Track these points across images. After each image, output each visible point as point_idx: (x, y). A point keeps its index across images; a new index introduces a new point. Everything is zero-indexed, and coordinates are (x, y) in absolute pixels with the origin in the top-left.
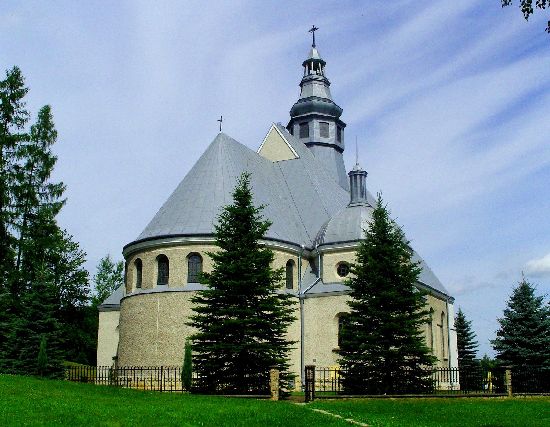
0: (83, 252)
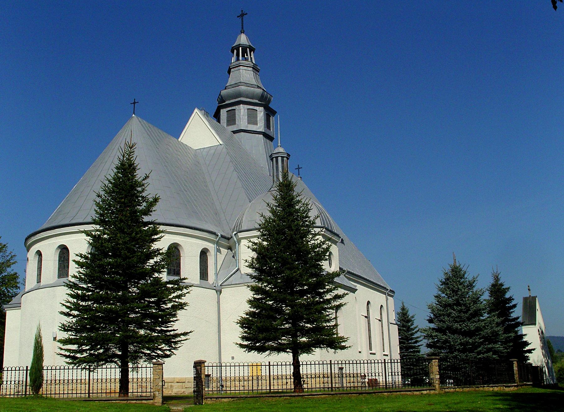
0: (13, 254)
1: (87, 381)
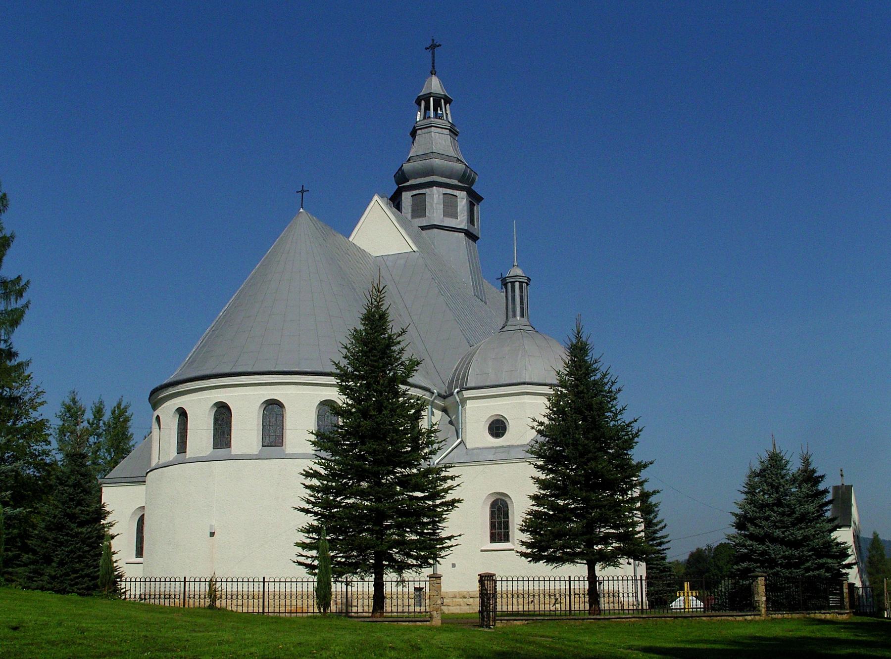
0: (39, 390)
1: (261, 593)
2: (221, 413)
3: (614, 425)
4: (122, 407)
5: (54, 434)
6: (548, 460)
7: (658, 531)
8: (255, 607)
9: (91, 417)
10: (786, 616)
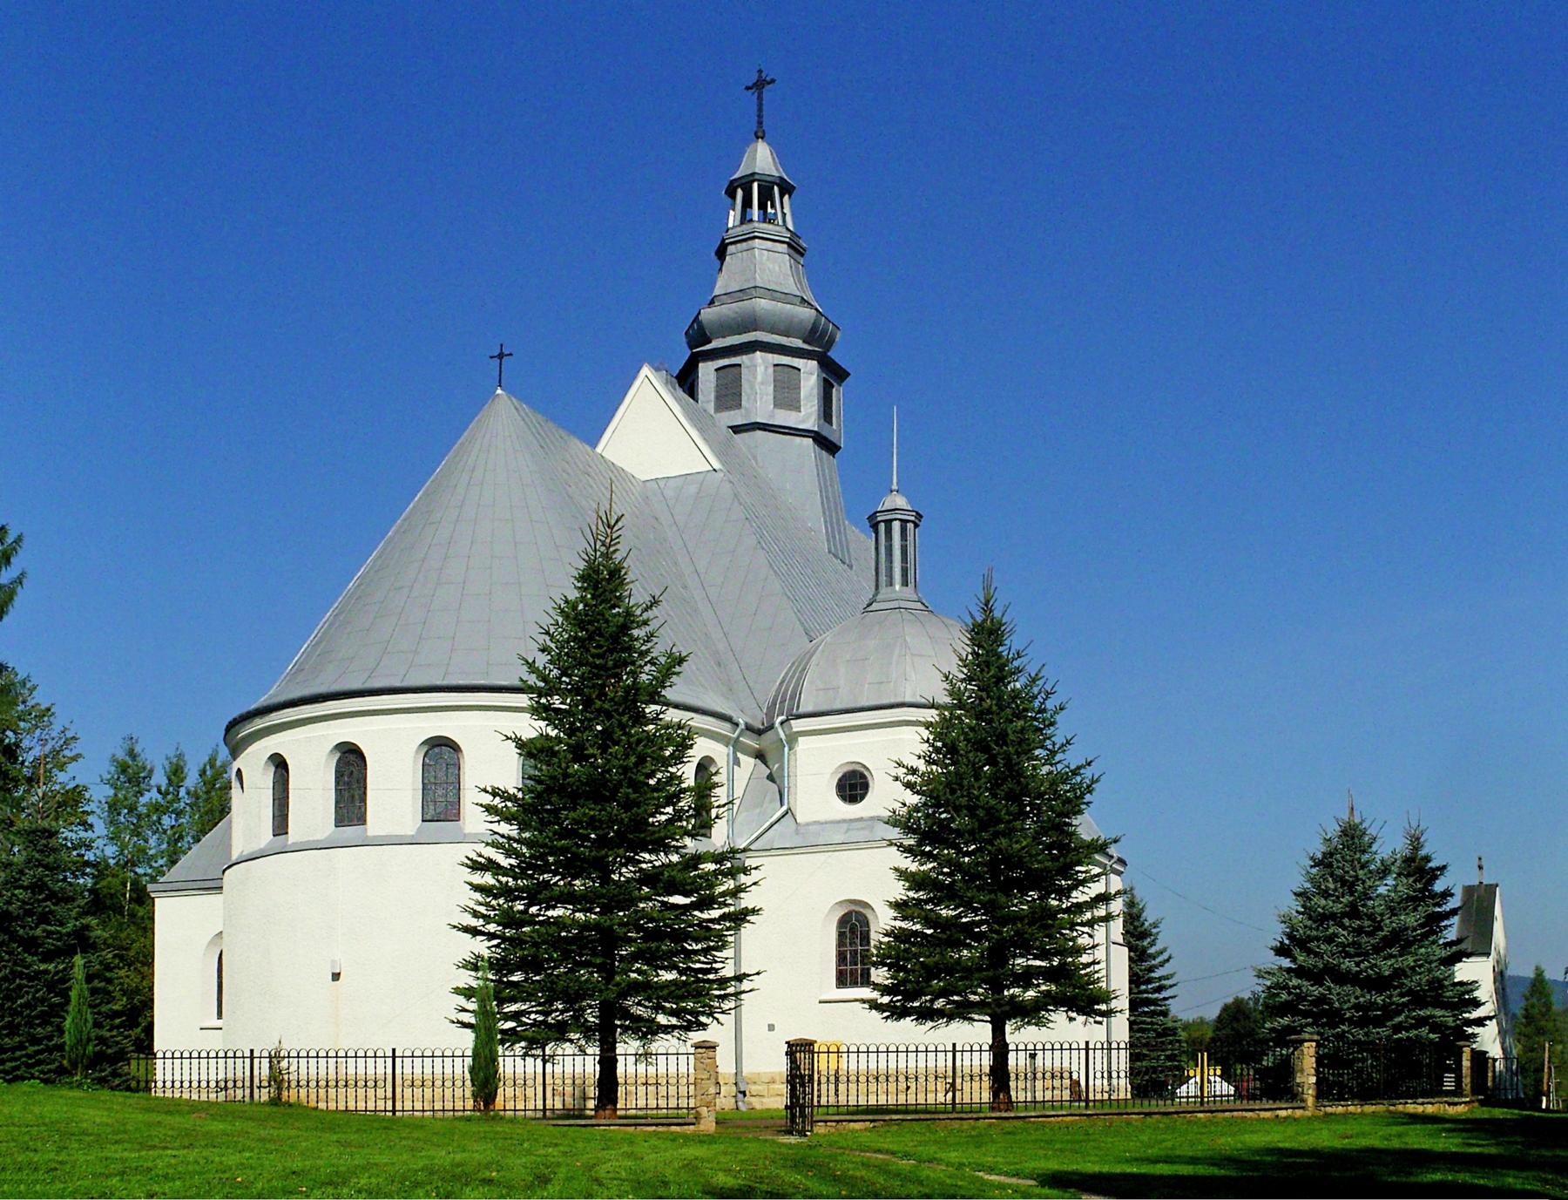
0: (69, 734)
2: (348, 764)
3: (1050, 773)
4: (218, 763)
5: (98, 811)
6: (926, 836)
7: (1156, 967)
8: (375, 1101)
9: (164, 783)
10: (1351, 1109)
